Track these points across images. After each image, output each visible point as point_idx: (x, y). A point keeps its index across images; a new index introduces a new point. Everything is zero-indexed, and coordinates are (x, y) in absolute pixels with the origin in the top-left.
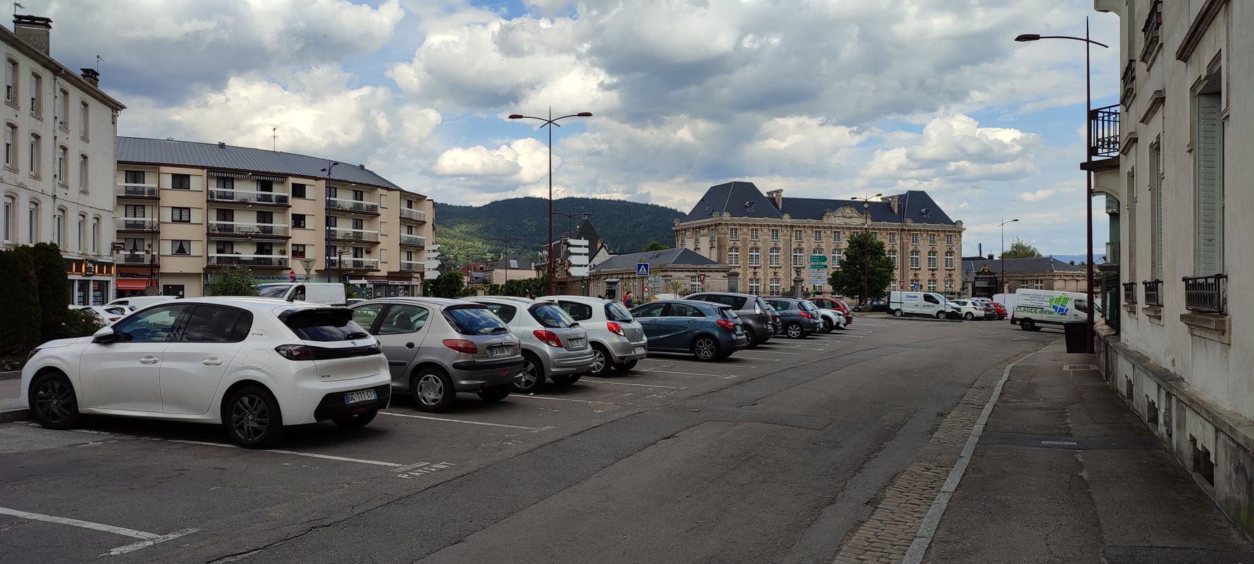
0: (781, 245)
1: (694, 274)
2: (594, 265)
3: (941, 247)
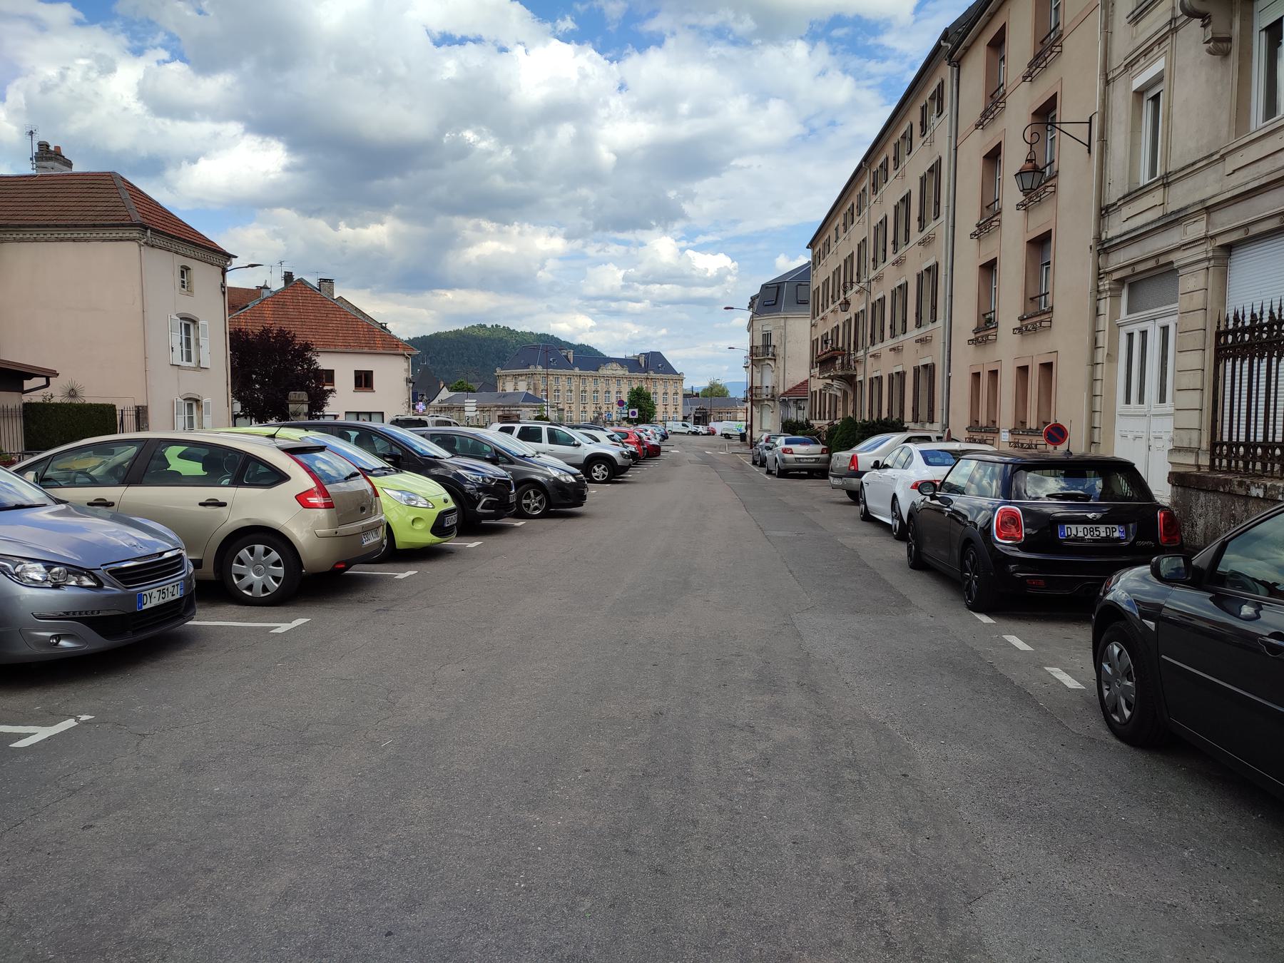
0: (573, 388)
1: (535, 409)
3: (671, 390)
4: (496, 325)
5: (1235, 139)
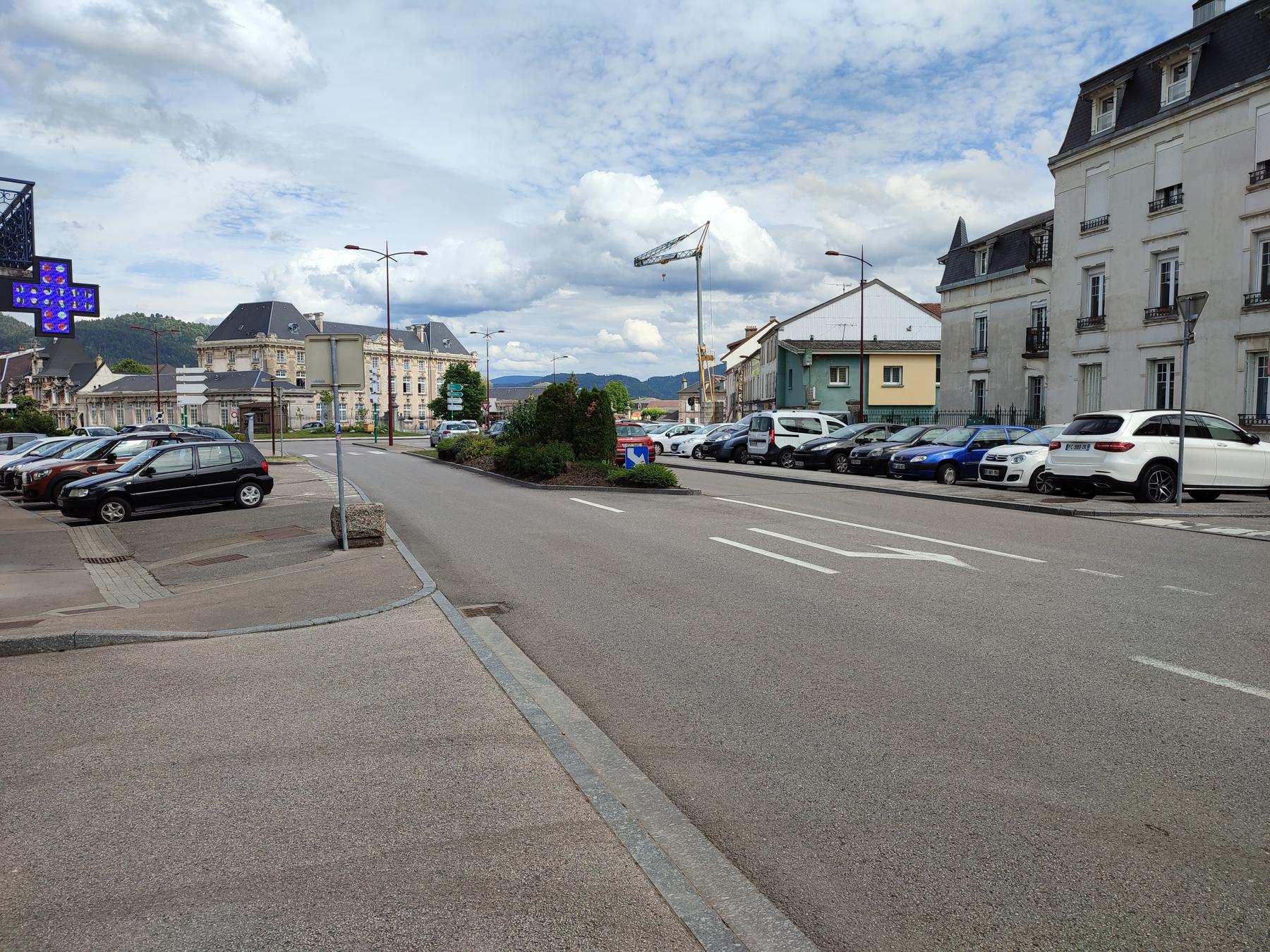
2: (99, 386)
4: (157, 315)
5: (1103, 113)
